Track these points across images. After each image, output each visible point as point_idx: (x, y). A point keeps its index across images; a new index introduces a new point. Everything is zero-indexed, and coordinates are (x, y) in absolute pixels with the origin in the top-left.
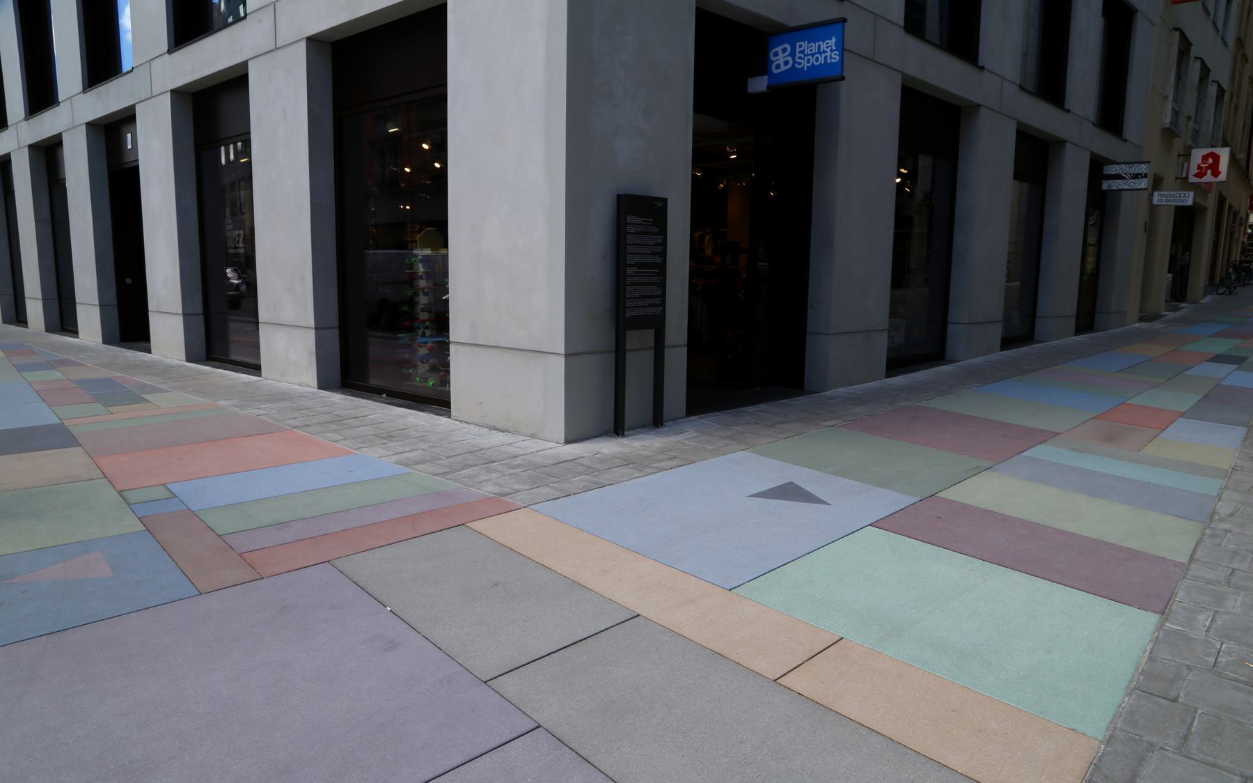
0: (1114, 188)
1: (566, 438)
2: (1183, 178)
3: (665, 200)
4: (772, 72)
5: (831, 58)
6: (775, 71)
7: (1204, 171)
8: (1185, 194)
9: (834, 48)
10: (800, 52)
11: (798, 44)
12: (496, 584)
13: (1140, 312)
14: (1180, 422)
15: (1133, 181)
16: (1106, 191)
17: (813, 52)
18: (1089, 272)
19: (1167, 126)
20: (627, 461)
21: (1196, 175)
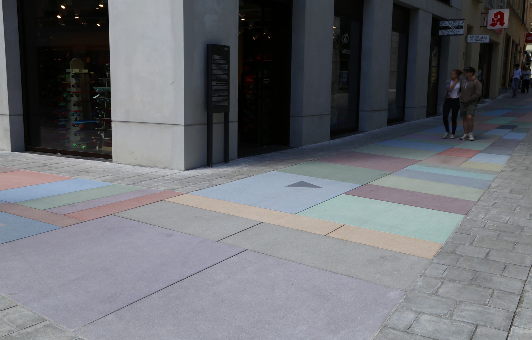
0: (446, 34)
1: (185, 168)
2: (483, 27)
3: (228, 47)
7: (495, 22)
8: (485, 36)
12: (197, 217)
15: (455, 30)
16: (441, 36)
20: (221, 176)
21: (491, 25)
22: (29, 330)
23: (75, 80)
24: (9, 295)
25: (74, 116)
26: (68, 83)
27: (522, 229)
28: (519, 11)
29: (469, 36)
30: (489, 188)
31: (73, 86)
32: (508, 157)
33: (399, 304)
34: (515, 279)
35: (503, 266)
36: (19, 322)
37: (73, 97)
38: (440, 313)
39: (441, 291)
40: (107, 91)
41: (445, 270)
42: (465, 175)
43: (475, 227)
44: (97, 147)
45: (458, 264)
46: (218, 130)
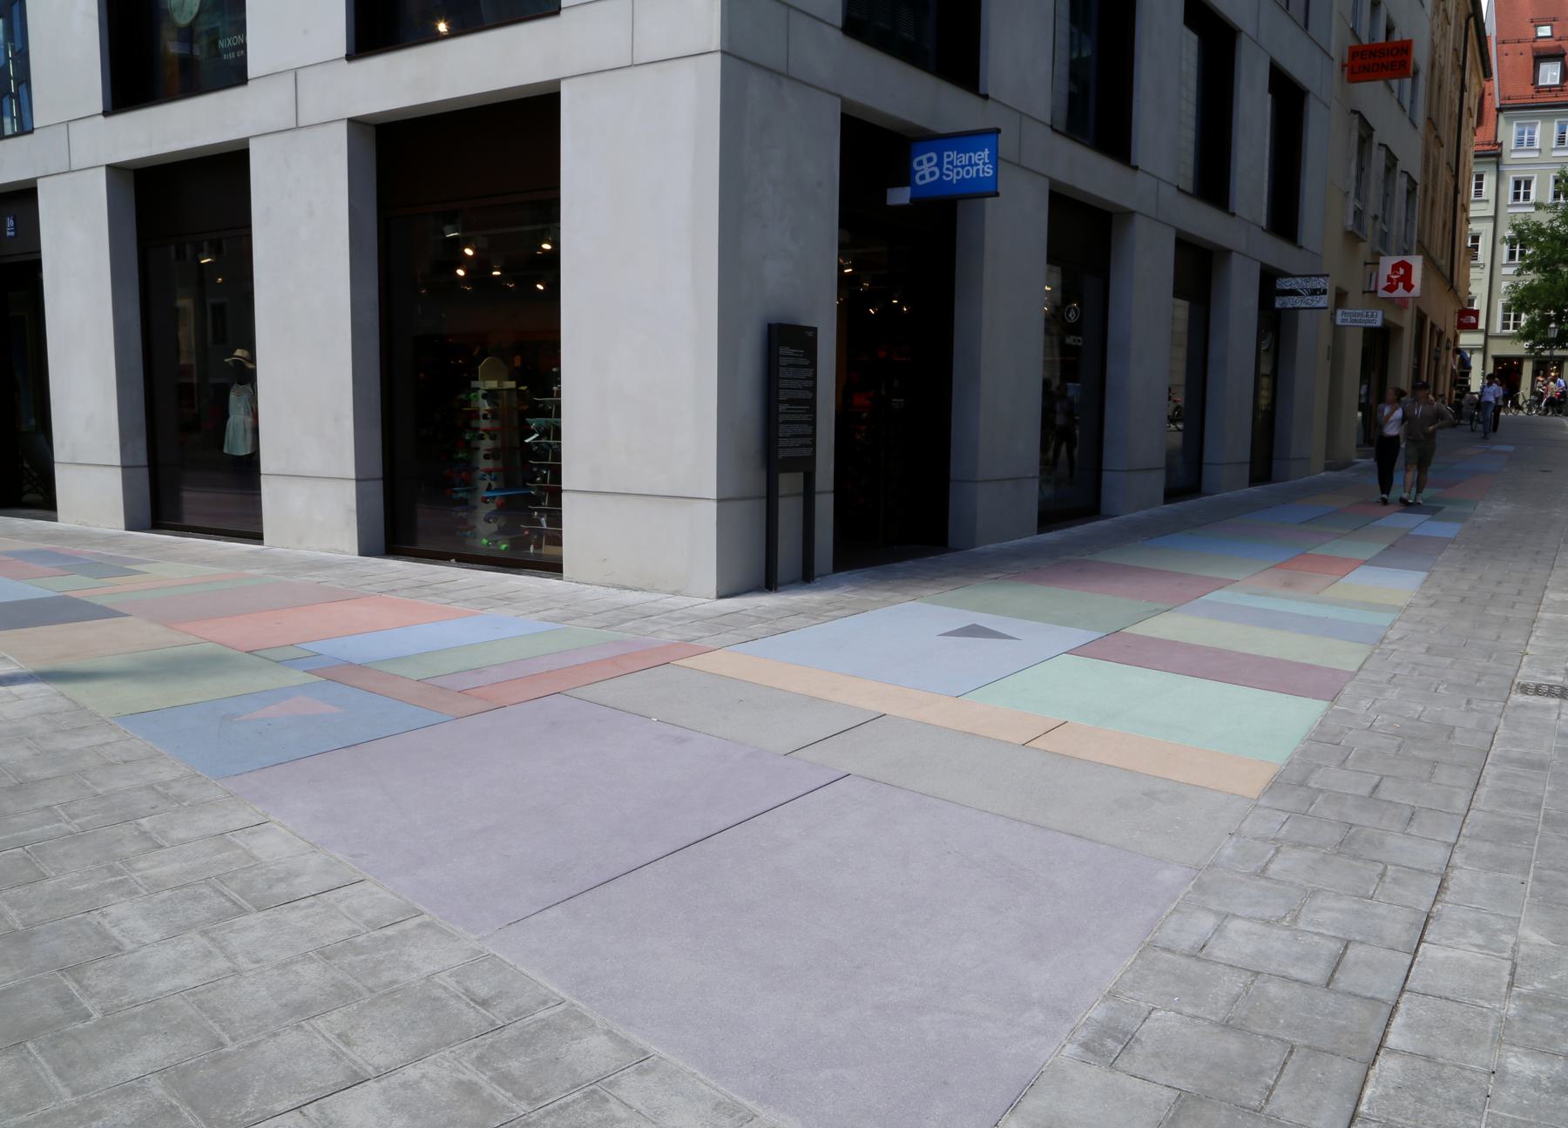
0: (1289, 306)
1: (717, 592)
2: (1370, 292)
3: (815, 330)
4: (915, 183)
5: (984, 171)
6: (919, 182)
7: (1394, 284)
9: (987, 161)
10: (948, 163)
11: (946, 154)
13: (1326, 459)
14: (1362, 570)
16: (1280, 310)
17: (963, 163)
18: (1263, 408)
19: (1350, 229)
21: (1386, 289)
22: (389, 932)
23: (489, 405)
24: (350, 858)
25: (485, 479)
26: (475, 411)
27: (1451, 731)
28: (1443, 262)
29: (1339, 312)
30: (1381, 642)
31: (485, 417)
32: (1423, 575)
33: (1181, 896)
34: (1433, 842)
35: (1407, 813)
36: (369, 914)
37: (483, 439)
38: (1271, 917)
39: (1274, 867)
40: (554, 426)
41: (1284, 823)
42: (1331, 613)
43: (1350, 729)
44: (532, 547)
45: (1311, 809)
46: (790, 510)
